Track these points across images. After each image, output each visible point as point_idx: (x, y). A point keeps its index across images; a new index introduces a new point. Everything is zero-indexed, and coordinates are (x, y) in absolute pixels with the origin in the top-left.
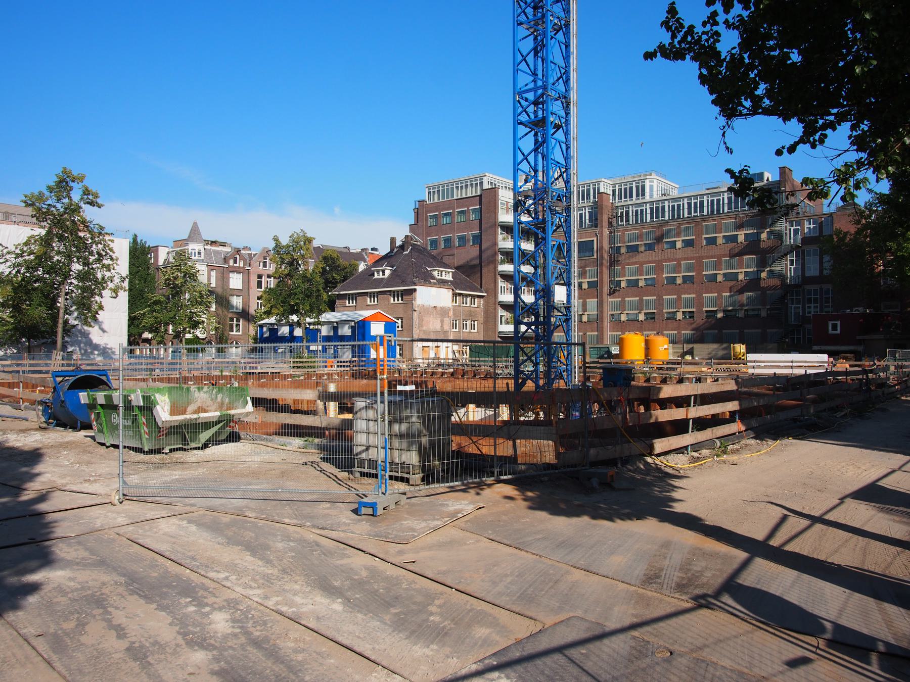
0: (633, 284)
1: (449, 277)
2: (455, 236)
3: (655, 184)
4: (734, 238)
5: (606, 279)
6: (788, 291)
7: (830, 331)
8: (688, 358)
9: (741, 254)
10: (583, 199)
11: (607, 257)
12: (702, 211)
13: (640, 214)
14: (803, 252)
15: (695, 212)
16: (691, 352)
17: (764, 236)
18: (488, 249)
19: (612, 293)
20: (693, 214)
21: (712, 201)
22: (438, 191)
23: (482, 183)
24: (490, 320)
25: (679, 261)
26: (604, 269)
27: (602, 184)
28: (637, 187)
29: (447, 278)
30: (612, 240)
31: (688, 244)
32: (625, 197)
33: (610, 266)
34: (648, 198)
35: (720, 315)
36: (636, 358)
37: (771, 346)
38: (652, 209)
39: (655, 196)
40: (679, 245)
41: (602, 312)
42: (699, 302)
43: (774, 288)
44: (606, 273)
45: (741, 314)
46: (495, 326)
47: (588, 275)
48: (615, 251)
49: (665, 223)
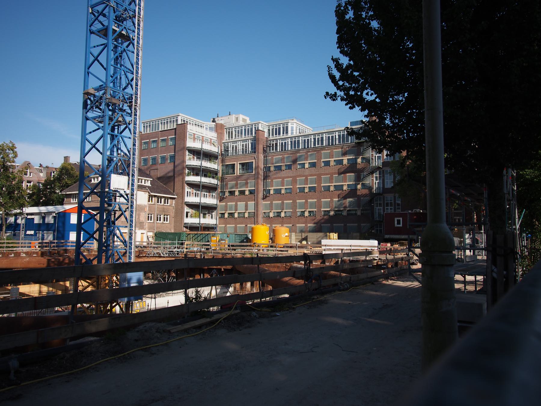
0: (278, 191)
1: (148, 184)
2: (159, 156)
3: (295, 126)
4: (340, 162)
5: (261, 188)
6: (373, 197)
7: (396, 225)
8: (304, 242)
9: (345, 172)
10: (248, 134)
11: (261, 173)
12: (322, 143)
13: (283, 146)
14: (383, 171)
15: (318, 144)
16: (306, 239)
17: (359, 160)
18: (179, 165)
19: (264, 198)
20: (317, 146)
21: (329, 137)
22: (150, 125)
23: (177, 120)
24: (179, 214)
25: (307, 177)
26: (260, 181)
27: (260, 124)
28: (283, 128)
29: (146, 185)
30: (266, 162)
31: (313, 165)
32: (248, 134)
33: (264, 179)
34: (290, 135)
35: (332, 213)
36: (263, 242)
37: (355, 234)
38: (291, 142)
39: (295, 134)
40: (307, 166)
41: (257, 211)
42: (319, 205)
43: (365, 196)
44: (261, 183)
45: (345, 213)
46: (182, 219)
47: (249, 185)
48: (267, 169)
49: (299, 151)
